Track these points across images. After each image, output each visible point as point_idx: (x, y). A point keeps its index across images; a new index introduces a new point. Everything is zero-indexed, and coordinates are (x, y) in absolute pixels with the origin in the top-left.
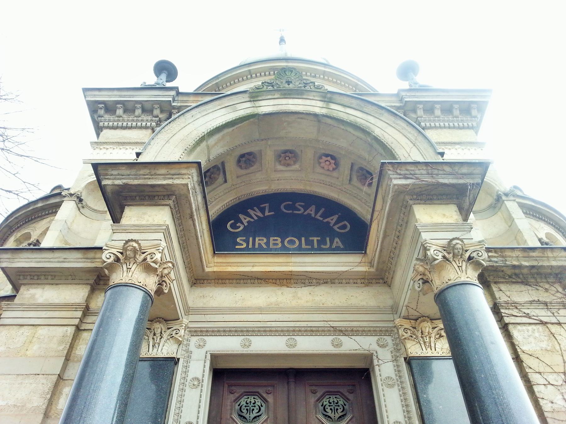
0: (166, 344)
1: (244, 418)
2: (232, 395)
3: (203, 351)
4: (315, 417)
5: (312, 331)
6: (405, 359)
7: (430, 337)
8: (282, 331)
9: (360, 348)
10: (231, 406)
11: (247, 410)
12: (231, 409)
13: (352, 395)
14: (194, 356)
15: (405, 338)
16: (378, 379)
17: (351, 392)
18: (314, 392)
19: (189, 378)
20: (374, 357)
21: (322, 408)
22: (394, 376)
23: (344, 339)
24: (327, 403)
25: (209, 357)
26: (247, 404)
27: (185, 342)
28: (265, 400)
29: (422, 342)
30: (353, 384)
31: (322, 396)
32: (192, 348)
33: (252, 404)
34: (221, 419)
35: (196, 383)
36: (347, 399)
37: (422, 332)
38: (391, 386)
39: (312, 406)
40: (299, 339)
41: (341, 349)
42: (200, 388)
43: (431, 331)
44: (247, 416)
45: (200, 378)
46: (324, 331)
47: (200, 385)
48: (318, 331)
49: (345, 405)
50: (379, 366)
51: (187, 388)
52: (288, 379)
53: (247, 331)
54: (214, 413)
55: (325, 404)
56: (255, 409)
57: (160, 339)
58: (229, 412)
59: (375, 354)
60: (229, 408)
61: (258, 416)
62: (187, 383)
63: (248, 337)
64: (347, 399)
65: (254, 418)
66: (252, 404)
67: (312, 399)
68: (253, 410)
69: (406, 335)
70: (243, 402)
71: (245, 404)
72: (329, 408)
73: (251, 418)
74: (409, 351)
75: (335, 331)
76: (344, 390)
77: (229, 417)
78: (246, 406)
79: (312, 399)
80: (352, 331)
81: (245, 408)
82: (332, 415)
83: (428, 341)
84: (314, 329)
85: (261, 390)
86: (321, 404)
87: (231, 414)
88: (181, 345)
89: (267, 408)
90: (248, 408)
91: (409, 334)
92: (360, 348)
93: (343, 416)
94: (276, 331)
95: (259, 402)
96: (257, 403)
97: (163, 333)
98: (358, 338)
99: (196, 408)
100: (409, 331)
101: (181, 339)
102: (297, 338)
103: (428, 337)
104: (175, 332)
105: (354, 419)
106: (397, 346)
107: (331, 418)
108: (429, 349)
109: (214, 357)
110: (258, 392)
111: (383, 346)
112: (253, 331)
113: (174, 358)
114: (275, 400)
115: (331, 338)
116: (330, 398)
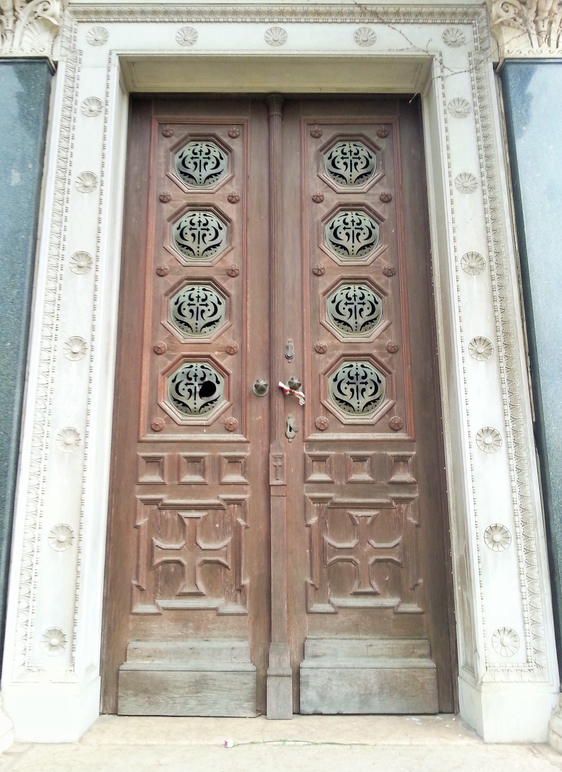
0: (27, 32)
1: (191, 176)
2: (166, 140)
3: (103, 51)
4: (315, 176)
5: (318, 13)
6: (495, 66)
7: (551, 23)
8: (258, 13)
9: (410, 46)
10: (167, 157)
11: (195, 164)
12: (167, 164)
13: (384, 140)
14: (87, 59)
15: (502, 23)
16: (439, 101)
17: (382, 136)
18: (316, 136)
19: (81, 99)
20: (436, 64)
21: (330, 162)
22: (468, 98)
23: (379, 29)
24: (339, 153)
25: (115, 61)
26: (196, 154)
27: (67, 34)
28: (227, 149)
29: (533, 31)
30: (388, 121)
31: (329, 143)
32: (82, 43)
33: (204, 155)
34: (149, 177)
35: (94, 107)
36: (374, 148)
37: (537, 12)
38: (460, 115)
39: (312, 159)
40: (292, 29)
41: (372, 47)
42: (102, 115)
43: (555, 8)
44: (196, 174)
45: (102, 98)
46: (340, 13)
47: (103, 110)
48: (329, 13)
49: (371, 157)
50: (443, 78)
51: (79, 116)
52: (269, 112)
53: (189, 13)
54: (135, 169)
55: (334, 156)
56: (209, 162)
57: (15, 22)
58: (163, 167)
59: (437, 57)
60: (162, 160)
61: (215, 175)
62: (78, 107)
63: (190, 25)
64: (374, 148)
65: (207, 178)
66: (203, 154)
67: (313, 147)
68: (206, 164)
69: (505, 16)
70: (187, 151)
71: (192, 155)
72: (342, 161)
73: (203, 178)
74: (506, 47)
75: (363, 13)
76: (371, 133)
77: (163, 175)
78: (192, 158)
79: (313, 147)
80: (397, 13)
81: (192, 161)
82: (348, 244)
83: (546, 28)
84: (322, 9)
85: (220, 133)
86: (328, 155)
87: (167, 170)
88: (59, 39)
89: (232, 162)
90: (197, 161)
91: (511, 13)
92: (410, 46)
93: (366, 174)
94: (247, 13)
95: (216, 152)
96: (212, 153)
97: (18, 9)
98: (406, 29)
99: (99, 151)
100: (511, 9)
101: (55, 22)
102: (288, 28)
103: (547, 22)
104: (41, 7)
105: (385, 180)
106: (481, 43)
107: (344, 178)
108: (545, 45)
109: (129, 65)
110: (214, 136)
111: (454, 44)
112: (200, 13)
113: (46, 58)
114: (245, 154)
115: (354, 28)
116: (346, 215)
